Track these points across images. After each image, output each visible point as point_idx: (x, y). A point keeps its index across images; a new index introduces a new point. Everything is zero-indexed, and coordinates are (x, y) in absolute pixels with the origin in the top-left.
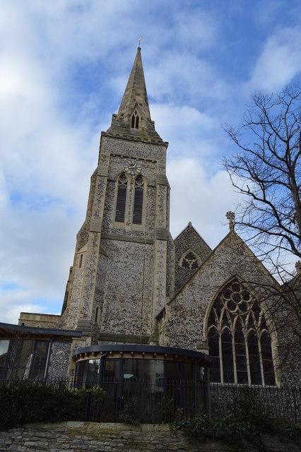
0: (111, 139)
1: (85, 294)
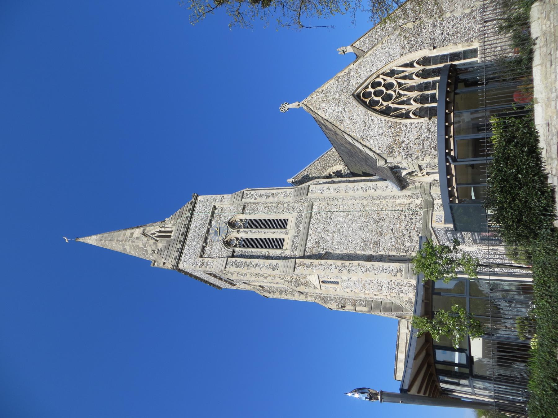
0: (182, 258)
1: (372, 273)
